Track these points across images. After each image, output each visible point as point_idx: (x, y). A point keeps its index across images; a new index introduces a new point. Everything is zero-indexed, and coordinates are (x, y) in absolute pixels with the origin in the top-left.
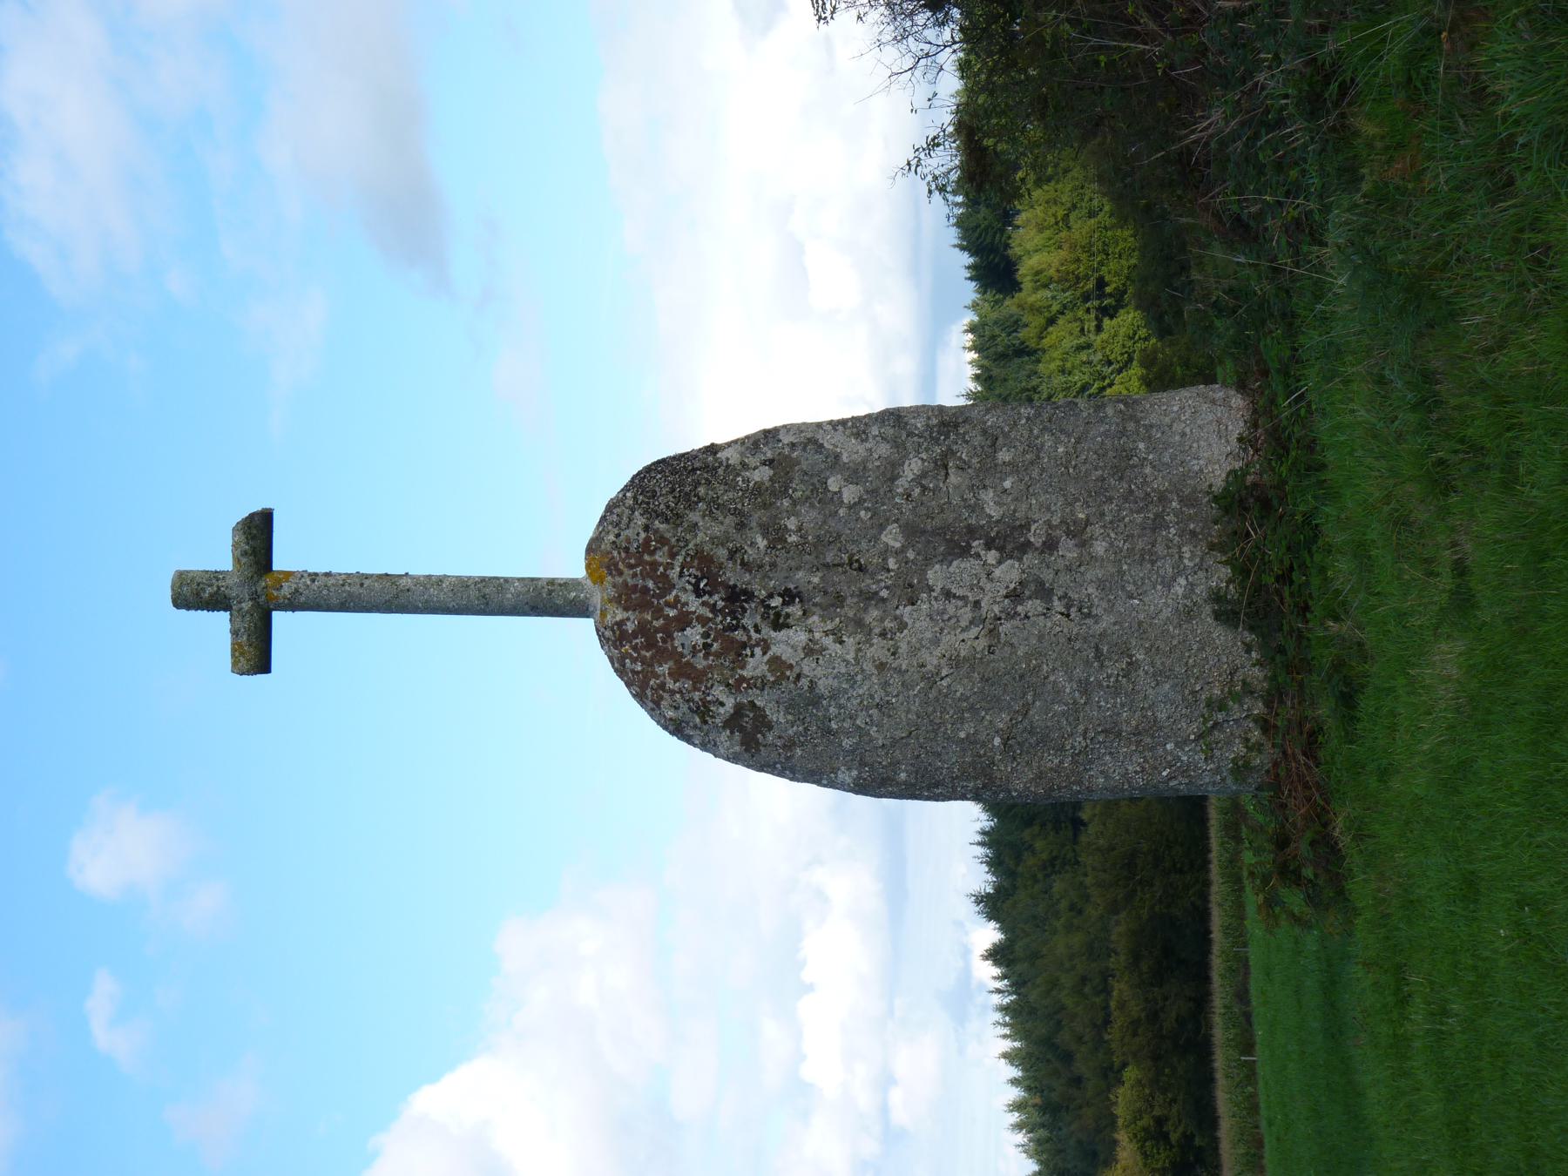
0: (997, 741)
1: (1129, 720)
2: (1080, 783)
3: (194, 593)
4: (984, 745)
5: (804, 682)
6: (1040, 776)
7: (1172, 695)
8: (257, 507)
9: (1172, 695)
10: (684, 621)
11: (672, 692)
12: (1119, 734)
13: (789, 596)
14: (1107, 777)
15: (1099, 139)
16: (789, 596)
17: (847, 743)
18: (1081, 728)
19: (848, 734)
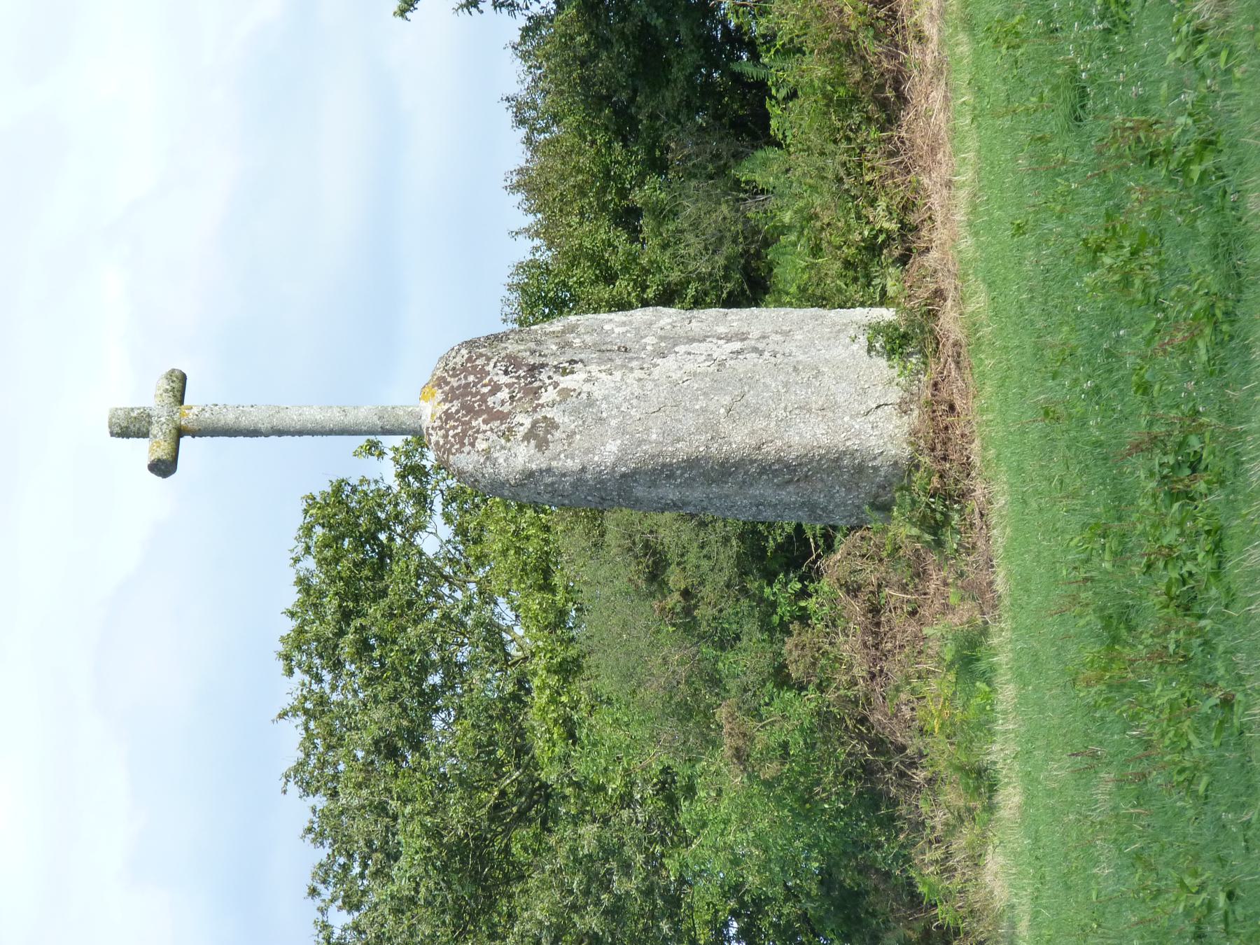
0: (722, 411)
1: (817, 402)
2: (781, 438)
3: (130, 428)
4: (712, 413)
5: (584, 396)
6: (753, 432)
7: (848, 389)
8: (153, 476)
9: (848, 389)
10: (496, 389)
11: (485, 432)
12: (809, 411)
13: (572, 362)
14: (801, 436)
15: (848, 443)
16: (572, 362)
17: (613, 423)
18: (783, 405)
19: (615, 417)
